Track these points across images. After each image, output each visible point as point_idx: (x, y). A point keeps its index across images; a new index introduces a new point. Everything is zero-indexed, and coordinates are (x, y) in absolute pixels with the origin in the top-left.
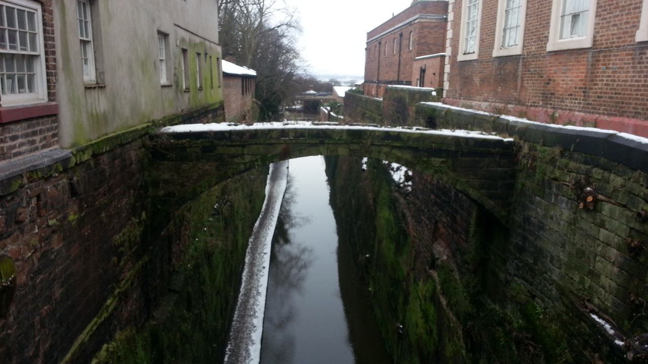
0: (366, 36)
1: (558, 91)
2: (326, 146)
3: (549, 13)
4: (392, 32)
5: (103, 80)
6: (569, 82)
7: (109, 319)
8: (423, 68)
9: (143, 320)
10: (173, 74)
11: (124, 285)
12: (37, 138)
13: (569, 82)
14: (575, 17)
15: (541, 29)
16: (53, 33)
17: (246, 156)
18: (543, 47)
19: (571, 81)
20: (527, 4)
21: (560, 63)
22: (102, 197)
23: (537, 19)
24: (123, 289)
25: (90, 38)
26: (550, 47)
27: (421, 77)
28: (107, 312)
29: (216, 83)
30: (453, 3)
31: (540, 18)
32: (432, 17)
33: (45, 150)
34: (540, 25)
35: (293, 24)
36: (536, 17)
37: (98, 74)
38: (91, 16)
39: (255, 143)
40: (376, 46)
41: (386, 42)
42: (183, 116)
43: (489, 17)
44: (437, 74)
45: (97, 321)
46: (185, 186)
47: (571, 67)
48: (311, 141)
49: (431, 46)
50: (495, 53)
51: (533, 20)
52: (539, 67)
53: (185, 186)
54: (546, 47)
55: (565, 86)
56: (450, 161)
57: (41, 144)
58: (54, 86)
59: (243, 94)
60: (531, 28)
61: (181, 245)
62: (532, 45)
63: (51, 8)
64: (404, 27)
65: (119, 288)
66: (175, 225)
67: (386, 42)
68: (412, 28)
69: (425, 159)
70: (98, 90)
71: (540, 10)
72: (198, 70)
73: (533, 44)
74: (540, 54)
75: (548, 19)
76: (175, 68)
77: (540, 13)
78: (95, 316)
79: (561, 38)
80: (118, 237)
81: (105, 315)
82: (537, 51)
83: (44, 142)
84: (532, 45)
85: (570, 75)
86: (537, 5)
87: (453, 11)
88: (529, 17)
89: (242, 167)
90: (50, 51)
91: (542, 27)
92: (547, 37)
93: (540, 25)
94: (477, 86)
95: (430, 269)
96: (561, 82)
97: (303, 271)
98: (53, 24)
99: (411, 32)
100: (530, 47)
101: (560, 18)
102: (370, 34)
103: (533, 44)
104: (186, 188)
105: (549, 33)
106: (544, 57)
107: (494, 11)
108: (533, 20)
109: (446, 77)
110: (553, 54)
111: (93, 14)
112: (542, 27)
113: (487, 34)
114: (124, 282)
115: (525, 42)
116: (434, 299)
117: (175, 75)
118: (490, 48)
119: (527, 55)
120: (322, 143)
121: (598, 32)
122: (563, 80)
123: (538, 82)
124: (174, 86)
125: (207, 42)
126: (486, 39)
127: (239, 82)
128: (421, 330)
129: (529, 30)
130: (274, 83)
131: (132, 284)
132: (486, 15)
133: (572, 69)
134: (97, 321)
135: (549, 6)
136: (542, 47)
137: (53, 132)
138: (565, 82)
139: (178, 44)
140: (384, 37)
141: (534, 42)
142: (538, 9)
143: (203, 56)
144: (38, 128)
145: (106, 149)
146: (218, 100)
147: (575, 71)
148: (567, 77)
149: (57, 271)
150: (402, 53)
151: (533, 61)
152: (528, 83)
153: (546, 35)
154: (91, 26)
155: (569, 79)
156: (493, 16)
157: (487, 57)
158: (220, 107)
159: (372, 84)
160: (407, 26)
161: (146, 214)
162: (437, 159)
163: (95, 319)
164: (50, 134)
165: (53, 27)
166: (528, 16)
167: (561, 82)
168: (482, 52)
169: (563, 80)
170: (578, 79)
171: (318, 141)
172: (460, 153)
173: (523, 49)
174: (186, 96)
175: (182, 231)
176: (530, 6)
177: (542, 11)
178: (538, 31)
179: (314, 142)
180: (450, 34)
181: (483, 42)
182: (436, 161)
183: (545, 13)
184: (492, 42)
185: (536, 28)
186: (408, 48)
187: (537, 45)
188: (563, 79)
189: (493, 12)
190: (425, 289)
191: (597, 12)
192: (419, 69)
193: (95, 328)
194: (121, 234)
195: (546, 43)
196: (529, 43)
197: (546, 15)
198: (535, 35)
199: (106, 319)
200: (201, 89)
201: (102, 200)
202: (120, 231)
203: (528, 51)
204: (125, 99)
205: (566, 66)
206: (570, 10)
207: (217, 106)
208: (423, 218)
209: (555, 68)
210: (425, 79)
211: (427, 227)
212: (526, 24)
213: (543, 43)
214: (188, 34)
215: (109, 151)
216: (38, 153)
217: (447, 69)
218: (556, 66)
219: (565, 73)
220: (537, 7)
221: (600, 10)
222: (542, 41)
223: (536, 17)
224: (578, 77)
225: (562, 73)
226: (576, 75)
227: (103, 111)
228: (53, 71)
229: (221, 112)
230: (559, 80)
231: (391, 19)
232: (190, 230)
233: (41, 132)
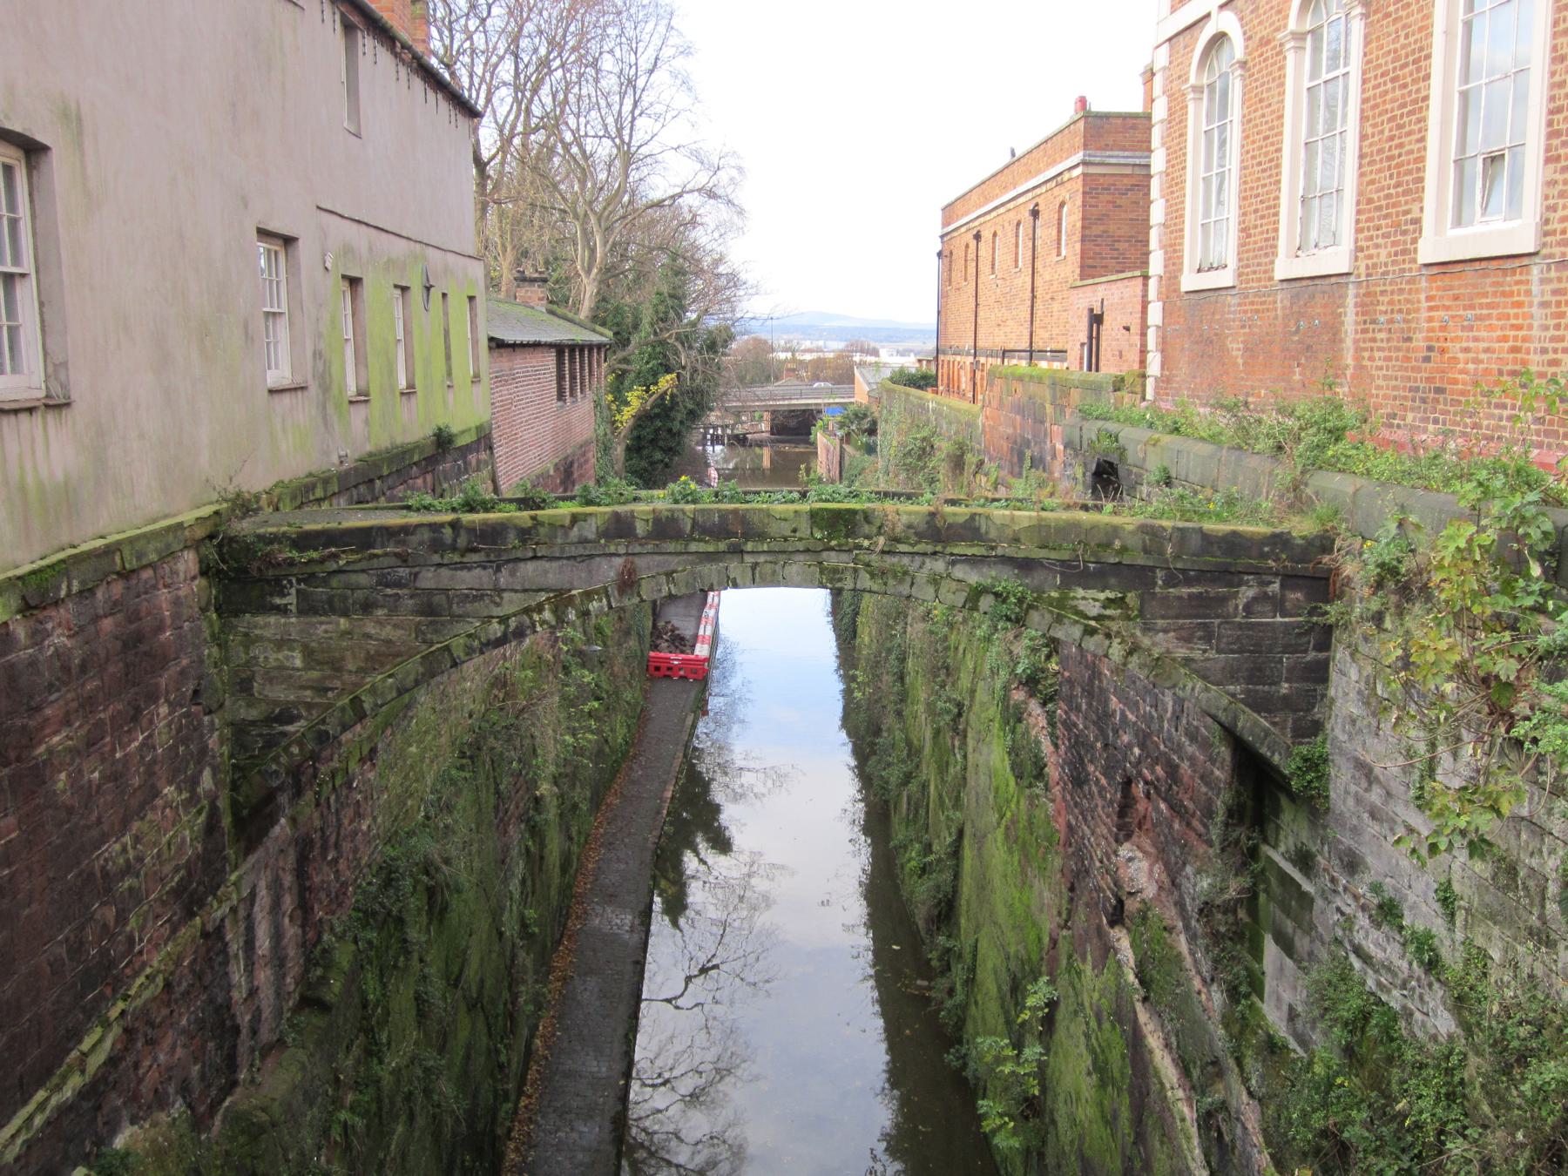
0: (938, 217)
1: (1455, 382)
2: (749, 559)
3: (1419, 150)
4: (1011, 205)
5: (64, 387)
6: (1483, 356)
7: (93, 1092)
8: (1097, 311)
9: (214, 1093)
10: (309, 353)
11: (142, 991)
13: (1483, 356)
14: (1494, 160)
15: (1402, 199)
18: (1408, 252)
19: (1487, 350)
20: (1362, 127)
21: (1456, 298)
22: (55, 733)
23: (1389, 168)
24: (139, 1002)
26: (1429, 250)
27: (1090, 338)
28: (83, 1072)
29: (464, 365)
30: (1162, 121)
31: (1398, 166)
32: (1122, 161)
34: (1397, 185)
35: (720, 192)
36: (1385, 164)
37: (50, 369)
38: (32, 201)
39: (530, 554)
40: (967, 246)
41: (995, 235)
42: (343, 477)
43: (1260, 164)
44: (1135, 329)
45: (48, 1099)
46: (328, 689)
47: (1485, 312)
48: (702, 547)
49: (1122, 246)
50: (1284, 268)
51: (1379, 171)
52: (1400, 311)
53: (328, 689)
54: (1416, 250)
55: (1471, 366)
56: (1132, 598)
59: (561, 396)
60: (1375, 196)
61: (342, 864)
62: (1377, 246)
64: (1043, 189)
65: (125, 998)
66: (318, 805)
67: (995, 235)
68: (1062, 193)
69: (1054, 594)
70: (44, 418)
71: (1396, 141)
72: (401, 336)
73: (1380, 241)
74: (1403, 270)
75: (1419, 170)
76: (319, 336)
77: (1396, 152)
78: (40, 1084)
79: (1458, 222)
80: (117, 847)
81: (75, 1082)
82: (1394, 263)
84: (1377, 246)
85: (1484, 334)
86: (1387, 127)
87: (1163, 144)
88: (1369, 164)
89: (496, 629)
91: (1405, 193)
92: (1417, 221)
93: (1397, 185)
94: (1235, 364)
95: (1112, 924)
96: (1461, 356)
99: (1062, 205)
100: (1372, 251)
101: (1452, 165)
102: (949, 212)
103: (1380, 241)
104: (330, 694)
105: (1422, 209)
106: (1411, 281)
107: (1272, 144)
108: (1379, 171)
109: (1152, 335)
110: (1435, 270)
111: (36, 197)
112: (1405, 193)
113: (1256, 211)
114: (141, 980)
115: (1361, 236)
116: (1122, 1016)
117: (317, 354)
118: (1266, 255)
119: (1368, 275)
120: (738, 551)
121: (1553, 208)
122: (1467, 350)
123: (1401, 354)
124: (314, 389)
125: (431, 252)
126: (1256, 227)
127: (550, 359)
128: (1086, 1112)
129: (1370, 201)
130: (654, 360)
131: (168, 986)
132: (1253, 157)
133: (1489, 316)
134: (48, 1099)
135: (1420, 131)
136: (1404, 252)
138: (1471, 355)
139: (328, 265)
140: (988, 218)
141: (1384, 236)
142: (1391, 139)
143: (417, 293)
145: (69, 587)
146: (473, 422)
147: (1495, 322)
148: (1476, 339)
150: (1038, 265)
151: (1382, 293)
152: (1371, 359)
153: (1415, 215)
154: (31, 251)
155: (1482, 345)
156: (1271, 161)
157: (1259, 280)
158: (479, 440)
159: (958, 358)
160: (1049, 185)
161: (214, 775)
162: (1092, 593)
163: (41, 1095)
166: (1366, 161)
167: (1461, 356)
168: (1248, 266)
169: (1467, 350)
170: (1506, 345)
171: (722, 546)
172: (1159, 573)
173: (1356, 259)
174: (358, 415)
175: (346, 822)
176: (1370, 131)
177: (1401, 145)
178: (1394, 205)
179: (711, 548)
180: (1157, 213)
181: (1249, 236)
182: (1090, 600)
183: (1411, 152)
184: (1271, 235)
185: (1388, 196)
186: (1054, 252)
187: (1394, 244)
188: (1465, 345)
189: (1272, 149)
190: (1098, 985)
191: (1548, 150)
192: (1086, 312)
193: (38, 1121)
194: (127, 839)
195: (1415, 241)
196: (1371, 238)
197: (1411, 157)
198: (1386, 217)
199: (82, 1094)
200: (409, 392)
201: (56, 739)
202: (125, 825)
203: (1370, 262)
204: (142, 436)
205: (1472, 307)
206: (1478, 146)
209: (1441, 313)
210: (1103, 344)
211: (1104, 798)
212: (1360, 184)
213: (1409, 238)
217: (1155, 315)
218: (1447, 308)
219: (1471, 329)
220: (1387, 133)
221: (1556, 142)
222: (1404, 233)
223: (1385, 164)
224: (1505, 339)
225: (1463, 329)
226: (1499, 333)
227: (60, 476)
229: (484, 456)
230: (1454, 348)
232: (375, 819)
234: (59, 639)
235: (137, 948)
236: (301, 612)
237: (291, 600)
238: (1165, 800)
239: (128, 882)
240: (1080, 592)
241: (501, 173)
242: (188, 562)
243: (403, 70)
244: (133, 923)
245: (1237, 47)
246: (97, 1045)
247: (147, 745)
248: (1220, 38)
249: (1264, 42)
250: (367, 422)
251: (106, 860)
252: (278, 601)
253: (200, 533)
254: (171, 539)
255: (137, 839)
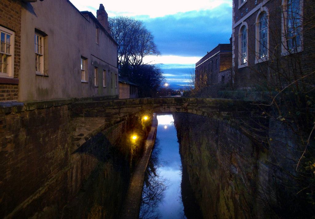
12: (5, 94)
16: (20, 46)
17: (121, 114)
25: (43, 54)
30: (234, 41)
33: (9, 101)
50: (256, 62)
57: (7, 97)
58: (18, 71)
63: (20, 35)
68: (217, 58)
70: (44, 78)
81: (38, 195)
83: (9, 97)
90: (17, 54)
97: (164, 191)
98: (20, 42)
99: (217, 60)
125: (110, 66)
137: (15, 93)
144: (6, 89)
149: (9, 164)
154: (43, 49)
163: (31, 196)
164: (13, 93)
165: (20, 44)
174: (96, 89)
182: (224, 114)
194: (52, 153)
207: (114, 97)
208: (225, 152)
214: (99, 60)
215: (47, 108)
216: (4, 101)
228: (18, 64)
231: (207, 55)
233: (8, 91)
234: (43, 115)
235: (52, 173)
236: (85, 117)
237: (83, 115)
238: (239, 155)
239: (50, 161)
240: (222, 112)
241: (121, 60)
242: (66, 107)
243: (106, 36)
244: (51, 168)
245: (247, 27)
246: (42, 190)
247: (56, 137)
248: (244, 26)
249: (252, 25)
250: (98, 91)
251: (48, 156)
252: (81, 115)
253: (69, 102)
254: (63, 103)
255: (53, 153)
